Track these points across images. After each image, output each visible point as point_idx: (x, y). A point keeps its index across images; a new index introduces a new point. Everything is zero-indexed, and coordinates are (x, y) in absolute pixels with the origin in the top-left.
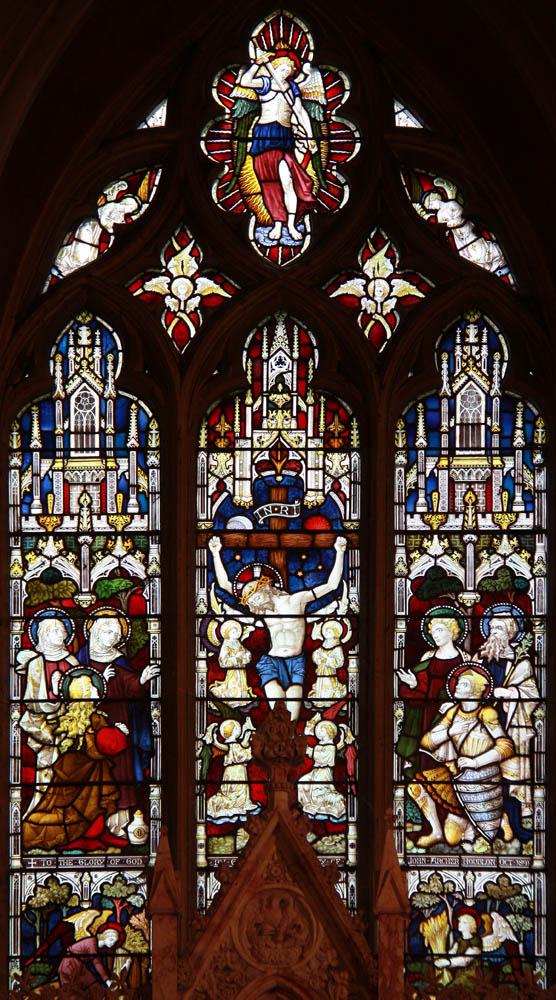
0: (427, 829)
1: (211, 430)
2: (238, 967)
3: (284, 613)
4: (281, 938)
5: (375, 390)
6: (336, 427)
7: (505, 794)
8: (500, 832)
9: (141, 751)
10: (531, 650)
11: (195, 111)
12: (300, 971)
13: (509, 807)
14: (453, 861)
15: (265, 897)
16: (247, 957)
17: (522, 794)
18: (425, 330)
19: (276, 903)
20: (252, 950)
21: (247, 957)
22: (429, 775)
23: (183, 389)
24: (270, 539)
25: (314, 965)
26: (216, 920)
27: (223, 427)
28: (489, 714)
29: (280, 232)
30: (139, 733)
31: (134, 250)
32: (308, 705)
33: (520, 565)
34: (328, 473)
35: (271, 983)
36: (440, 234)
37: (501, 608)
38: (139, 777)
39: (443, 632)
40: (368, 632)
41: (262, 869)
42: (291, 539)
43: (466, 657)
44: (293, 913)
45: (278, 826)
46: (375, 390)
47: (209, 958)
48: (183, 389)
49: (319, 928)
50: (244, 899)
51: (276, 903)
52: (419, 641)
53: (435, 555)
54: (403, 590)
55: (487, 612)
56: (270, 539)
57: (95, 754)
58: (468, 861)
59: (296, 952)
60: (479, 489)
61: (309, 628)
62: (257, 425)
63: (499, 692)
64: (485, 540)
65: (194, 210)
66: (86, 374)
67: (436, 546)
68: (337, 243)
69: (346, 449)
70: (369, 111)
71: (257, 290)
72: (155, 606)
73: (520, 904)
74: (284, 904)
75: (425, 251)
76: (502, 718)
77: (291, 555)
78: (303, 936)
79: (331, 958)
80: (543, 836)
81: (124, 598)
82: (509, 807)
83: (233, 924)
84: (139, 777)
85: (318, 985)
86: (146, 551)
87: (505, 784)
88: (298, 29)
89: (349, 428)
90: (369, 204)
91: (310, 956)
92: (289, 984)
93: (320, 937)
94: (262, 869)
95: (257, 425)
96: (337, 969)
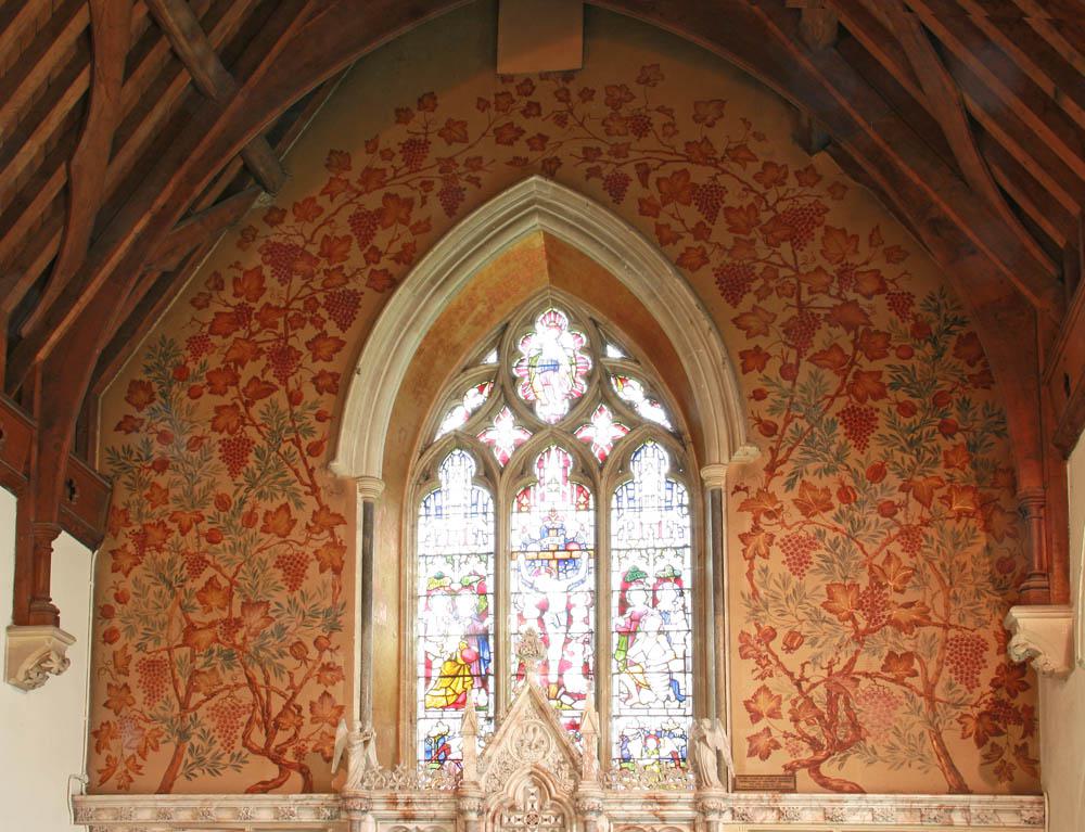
0: (630, 696)
1: (519, 502)
2: (510, 762)
3: (554, 588)
4: (533, 747)
5: (598, 477)
6: (582, 499)
7: (672, 680)
8: (668, 698)
9: (484, 660)
10: (684, 606)
11: (509, 354)
12: (543, 764)
13: (673, 683)
14: (644, 712)
15: (525, 727)
16: (515, 757)
17: (679, 677)
18: (624, 455)
19: (531, 729)
20: (518, 753)
21: (515, 757)
22: (632, 669)
23: (504, 480)
24: (550, 555)
25: (551, 760)
26: (497, 737)
27: (525, 501)
28: (662, 638)
29: (552, 406)
30: (483, 651)
31: (482, 418)
32: (569, 636)
33: (677, 564)
34: (580, 524)
35: (529, 771)
36: (630, 406)
37: (667, 585)
38: (483, 672)
39: (637, 598)
40: (599, 597)
41: (523, 713)
42: (560, 555)
43: (650, 610)
44: (539, 734)
45: (530, 690)
46: (598, 477)
47: (494, 758)
48: (504, 480)
49: (553, 741)
50: (513, 727)
51: (531, 729)
52: (624, 605)
53: (633, 561)
54: (616, 582)
55: (660, 587)
56: (550, 555)
57: (462, 662)
58: (652, 712)
59: (541, 754)
60: (656, 527)
61: (569, 597)
62: (543, 500)
63: (667, 628)
64: (659, 552)
65: (505, 391)
66: (458, 472)
67: (634, 555)
68: (581, 408)
69: (587, 509)
70: (595, 350)
71: (542, 435)
72: (490, 589)
73: (679, 732)
74: (534, 730)
75: (625, 414)
76: (669, 641)
77: (564, 560)
78: (546, 745)
79: (559, 757)
80: (691, 699)
81: (475, 585)
82: (673, 683)
83: (507, 740)
84: (483, 672)
85: (553, 771)
86: (486, 562)
87: (670, 673)
88: (560, 316)
89: (588, 499)
90: (598, 390)
91: (548, 756)
92: (538, 771)
93: (554, 747)
94: (523, 713)
95: (543, 500)
96: (564, 763)
